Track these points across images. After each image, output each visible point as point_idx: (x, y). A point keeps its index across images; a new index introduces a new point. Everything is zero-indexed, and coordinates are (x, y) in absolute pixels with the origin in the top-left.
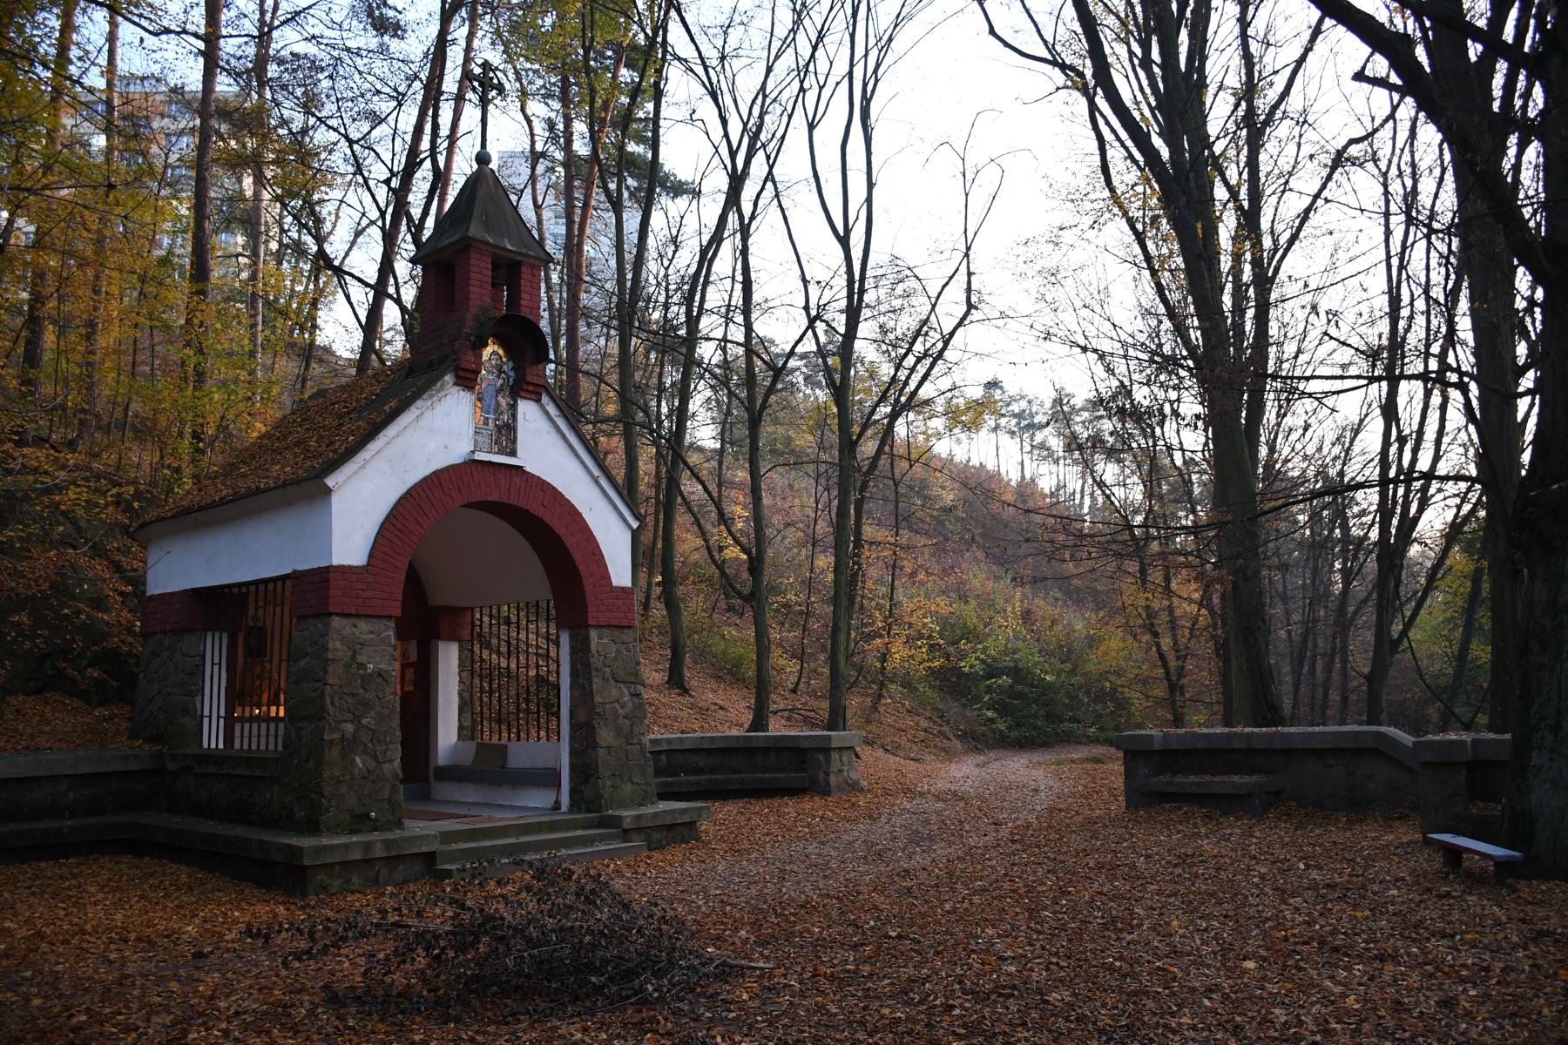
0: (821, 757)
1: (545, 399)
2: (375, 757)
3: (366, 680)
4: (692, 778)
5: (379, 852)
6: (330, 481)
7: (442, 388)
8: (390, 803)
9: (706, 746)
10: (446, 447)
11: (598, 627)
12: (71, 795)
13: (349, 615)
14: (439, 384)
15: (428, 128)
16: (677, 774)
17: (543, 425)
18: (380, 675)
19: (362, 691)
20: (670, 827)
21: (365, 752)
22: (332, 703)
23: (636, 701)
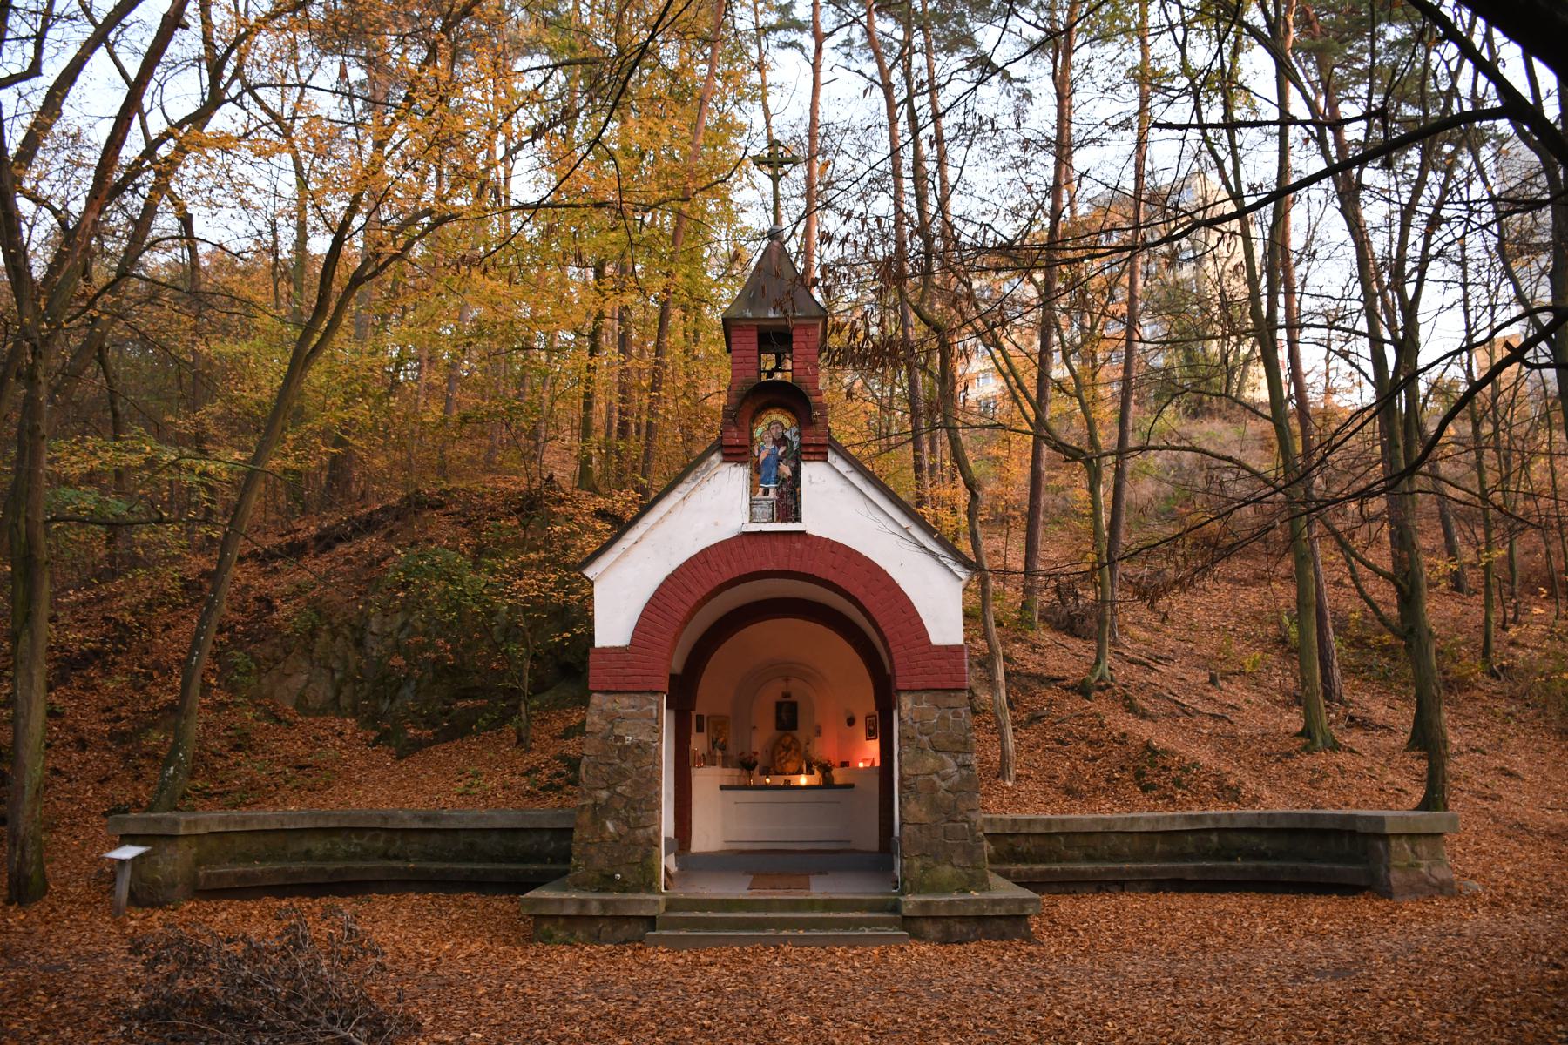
0: (1381, 845)
1: (832, 457)
2: (627, 823)
3: (624, 751)
4: (1252, 864)
5: (594, 910)
6: (590, 573)
7: (707, 468)
8: (642, 867)
9: (1264, 825)
10: (716, 524)
11: (911, 691)
12: (552, 845)
13: (608, 692)
14: (704, 466)
15: (1232, 180)
16: (1231, 858)
17: (836, 484)
18: (639, 747)
19: (618, 761)
20: (981, 919)
21: (617, 818)
22: (587, 772)
23: (964, 772)
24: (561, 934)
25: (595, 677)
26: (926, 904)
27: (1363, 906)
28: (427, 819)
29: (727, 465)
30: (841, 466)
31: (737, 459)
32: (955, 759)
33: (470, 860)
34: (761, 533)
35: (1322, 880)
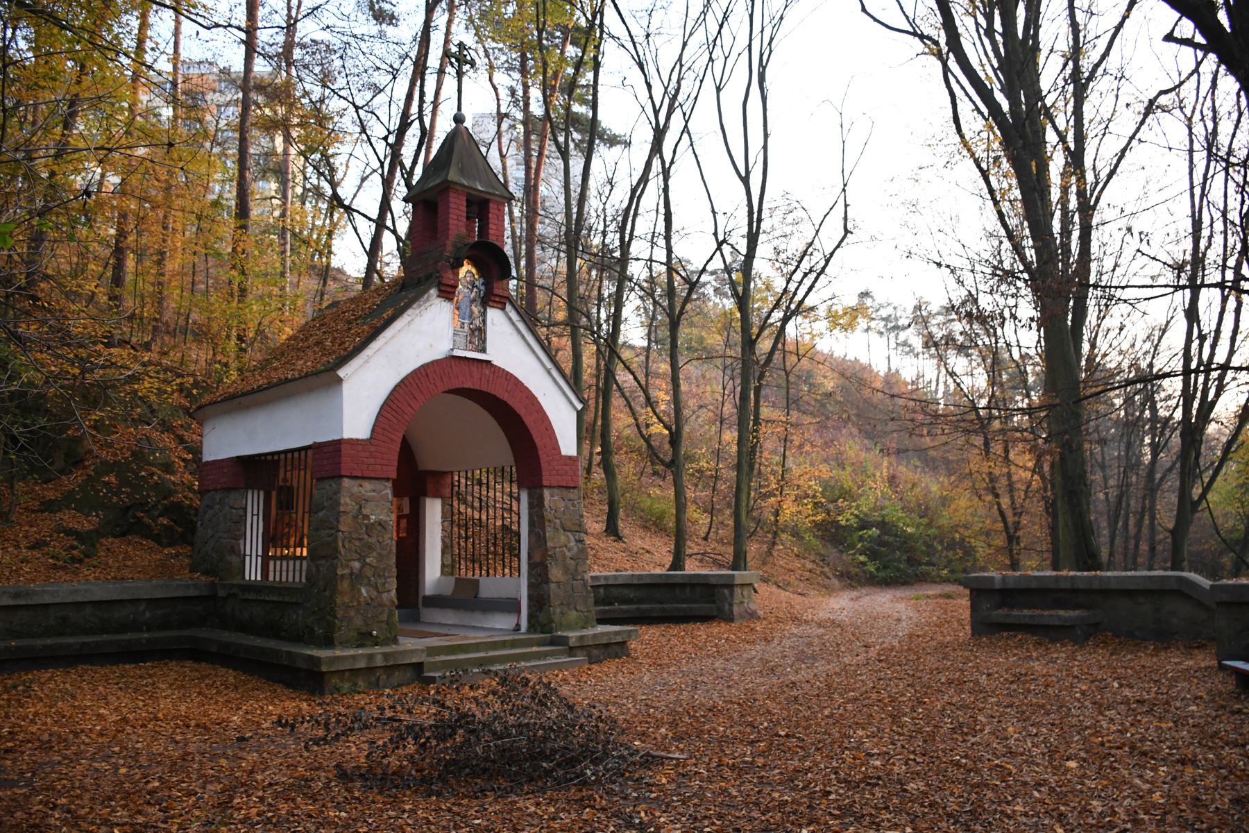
1: (508, 307)
2: (376, 588)
3: (369, 528)
4: (624, 607)
5: (379, 662)
6: (342, 373)
7: (428, 300)
9: (635, 582)
10: (431, 346)
11: (550, 487)
14: (426, 296)
18: (380, 524)
19: (366, 536)
21: (369, 584)
23: (580, 546)
24: (347, 685)
25: (347, 466)
26: (581, 638)
27: (716, 629)
28: (17, 595)
29: (440, 299)
30: (514, 315)
31: (446, 295)
32: (574, 536)
33: (61, 634)
34: (465, 358)
35: (681, 614)
